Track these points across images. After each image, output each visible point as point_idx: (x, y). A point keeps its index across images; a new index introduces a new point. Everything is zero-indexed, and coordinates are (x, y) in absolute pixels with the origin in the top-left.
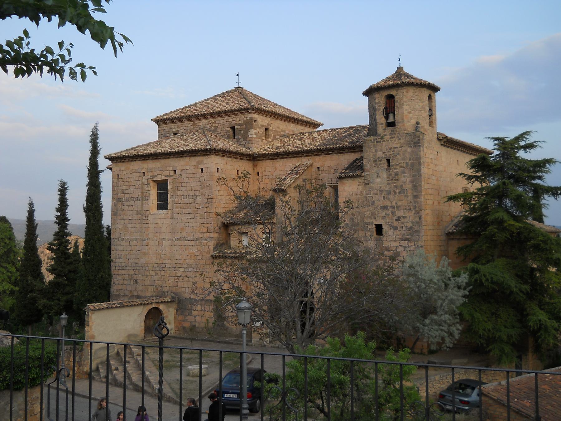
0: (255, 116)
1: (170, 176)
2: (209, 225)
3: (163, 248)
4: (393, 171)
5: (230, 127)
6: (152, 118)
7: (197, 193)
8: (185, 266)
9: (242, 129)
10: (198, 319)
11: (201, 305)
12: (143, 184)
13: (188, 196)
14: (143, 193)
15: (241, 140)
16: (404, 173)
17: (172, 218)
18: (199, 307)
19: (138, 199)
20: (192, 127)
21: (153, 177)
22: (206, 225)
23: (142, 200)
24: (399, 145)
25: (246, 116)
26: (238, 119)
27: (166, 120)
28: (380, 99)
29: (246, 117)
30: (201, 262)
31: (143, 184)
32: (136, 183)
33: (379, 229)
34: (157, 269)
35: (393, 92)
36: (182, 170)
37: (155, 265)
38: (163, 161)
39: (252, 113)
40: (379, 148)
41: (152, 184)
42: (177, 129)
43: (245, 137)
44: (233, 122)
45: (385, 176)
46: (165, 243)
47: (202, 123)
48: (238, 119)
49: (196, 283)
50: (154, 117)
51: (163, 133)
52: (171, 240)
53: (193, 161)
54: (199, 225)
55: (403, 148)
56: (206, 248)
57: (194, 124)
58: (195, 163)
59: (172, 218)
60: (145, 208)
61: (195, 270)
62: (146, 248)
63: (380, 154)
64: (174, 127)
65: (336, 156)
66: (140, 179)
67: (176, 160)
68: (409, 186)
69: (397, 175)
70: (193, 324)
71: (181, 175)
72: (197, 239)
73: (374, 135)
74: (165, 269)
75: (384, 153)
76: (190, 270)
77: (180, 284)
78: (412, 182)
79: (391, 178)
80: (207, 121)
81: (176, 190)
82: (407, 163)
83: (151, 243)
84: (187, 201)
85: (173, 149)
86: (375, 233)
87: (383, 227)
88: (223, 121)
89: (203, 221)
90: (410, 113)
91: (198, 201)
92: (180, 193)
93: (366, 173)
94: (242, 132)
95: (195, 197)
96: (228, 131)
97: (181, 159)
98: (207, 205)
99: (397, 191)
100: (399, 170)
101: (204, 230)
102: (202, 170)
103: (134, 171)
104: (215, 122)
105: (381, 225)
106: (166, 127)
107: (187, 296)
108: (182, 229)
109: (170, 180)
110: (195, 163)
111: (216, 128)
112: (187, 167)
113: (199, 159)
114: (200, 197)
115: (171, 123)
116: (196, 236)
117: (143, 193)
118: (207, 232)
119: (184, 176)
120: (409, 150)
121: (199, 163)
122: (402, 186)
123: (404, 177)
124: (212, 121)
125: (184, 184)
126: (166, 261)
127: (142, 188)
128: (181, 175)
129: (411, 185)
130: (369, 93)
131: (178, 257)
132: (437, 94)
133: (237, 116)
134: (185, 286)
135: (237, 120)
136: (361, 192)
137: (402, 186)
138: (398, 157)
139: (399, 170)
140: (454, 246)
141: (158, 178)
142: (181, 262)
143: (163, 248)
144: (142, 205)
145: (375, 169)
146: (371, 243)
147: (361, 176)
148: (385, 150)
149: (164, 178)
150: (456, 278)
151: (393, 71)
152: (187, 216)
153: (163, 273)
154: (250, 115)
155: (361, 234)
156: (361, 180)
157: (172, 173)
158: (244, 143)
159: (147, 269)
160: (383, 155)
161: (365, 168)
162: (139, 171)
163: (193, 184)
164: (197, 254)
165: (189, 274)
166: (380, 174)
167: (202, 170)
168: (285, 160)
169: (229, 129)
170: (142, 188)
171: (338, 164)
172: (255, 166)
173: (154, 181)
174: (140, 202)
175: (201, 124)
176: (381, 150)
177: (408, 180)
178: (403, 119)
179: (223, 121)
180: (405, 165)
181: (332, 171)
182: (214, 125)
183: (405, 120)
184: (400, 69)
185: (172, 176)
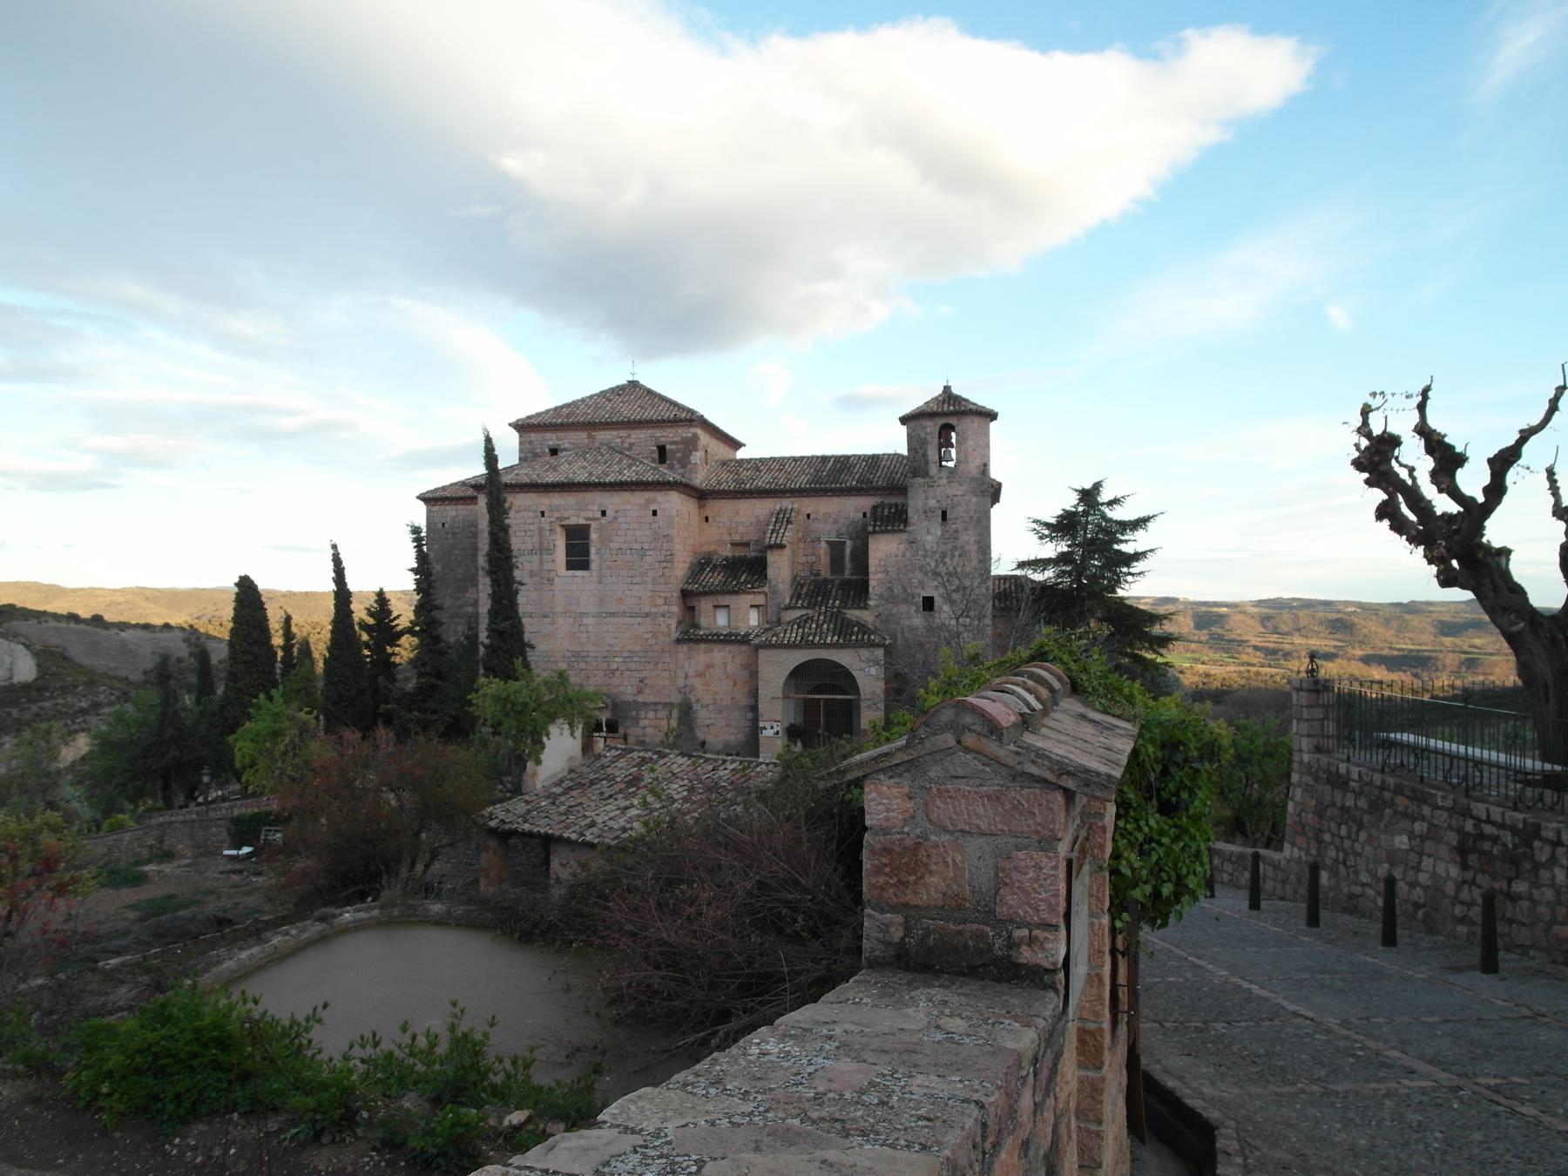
0: (699, 431)
1: (595, 519)
2: (669, 595)
3: (583, 628)
4: (951, 527)
5: (658, 447)
6: (511, 421)
7: (646, 546)
8: (626, 654)
9: (679, 450)
10: (649, 731)
11: (656, 711)
12: (541, 529)
13: (628, 551)
14: (541, 543)
15: (677, 466)
16: (966, 529)
17: (600, 582)
18: (651, 714)
19: (531, 552)
20: (586, 441)
21: (562, 519)
22: (663, 595)
23: (541, 554)
24: (959, 493)
25: (686, 430)
26: (671, 435)
27: (539, 425)
28: (932, 427)
29: (687, 432)
30: (655, 648)
31: (541, 529)
32: (527, 527)
33: (928, 604)
34: (573, 659)
35: (953, 421)
36: (617, 511)
37: (568, 654)
38: (581, 495)
39: (696, 426)
40: (931, 494)
41: (559, 530)
42: (556, 442)
43: (684, 462)
44: (663, 439)
45: (939, 533)
46: (585, 621)
47: (603, 436)
48: (671, 435)
49: (645, 678)
50: (513, 420)
51: (528, 446)
52: (599, 615)
53: (639, 498)
54: (650, 594)
55: (966, 497)
56: (664, 628)
57: (589, 436)
58: (642, 502)
59: (600, 582)
60: (547, 566)
61: (644, 660)
62: (551, 628)
63: (932, 503)
64: (552, 439)
65: (836, 500)
66: (536, 521)
67: (606, 494)
68: (973, 548)
69: (956, 531)
70: (641, 738)
71: (615, 518)
72: (647, 615)
73: (924, 477)
74: (589, 660)
75: (938, 502)
76: (634, 659)
77: (615, 681)
78: (978, 542)
79: (947, 536)
80: (614, 433)
81: (605, 541)
82: (971, 517)
83: (560, 621)
84: (628, 558)
85: (719, 483)
86: (921, 608)
87: (936, 599)
88: (643, 436)
89: (658, 587)
90: (974, 450)
91: (649, 559)
92: (612, 545)
93: (911, 528)
94: (679, 455)
95: (642, 553)
96: (652, 452)
97: (615, 494)
98: (665, 564)
99: (957, 553)
100: (959, 525)
101: (660, 601)
102: (655, 513)
103: (522, 508)
104: (629, 436)
105: (932, 598)
106: (533, 436)
107: (630, 699)
108: (619, 600)
109: (594, 525)
110: (642, 502)
111: (631, 445)
112: (627, 507)
113: (648, 495)
114: (652, 553)
115: (548, 431)
116: (646, 609)
117: (541, 543)
118: (665, 604)
119: (620, 520)
120: (974, 500)
121: (648, 502)
122: (963, 547)
123: (967, 535)
124: (623, 433)
125: (622, 533)
126: (590, 648)
127: (541, 535)
128: (615, 518)
129: (976, 546)
130: (904, 420)
131: (612, 641)
132: (993, 425)
133: (669, 430)
134: (625, 683)
135: (669, 436)
136: (904, 553)
137: (963, 547)
138: (959, 508)
139: (959, 525)
140: (182, 650)
141: (573, 521)
142: (617, 648)
143: (583, 628)
144: (541, 562)
145: (925, 523)
146: (918, 621)
147: (904, 531)
148: (940, 498)
149: (582, 521)
150: (52, 722)
151: (938, 391)
152: (629, 580)
153: (583, 665)
154: (693, 430)
155: (903, 608)
156: (904, 536)
157: (599, 514)
158: (682, 471)
159: (552, 659)
160: (938, 505)
161: (910, 520)
162: (534, 508)
163: (637, 533)
164: (646, 636)
165: (632, 666)
166: (932, 530)
167: (655, 513)
168: (753, 501)
169: (655, 448)
170: (541, 535)
171: (839, 512)
172: (701, 507)
173: (563, 526)
174: (536, 558)
175: (603, 437)
176: (934, 498)
177: (972, 539)
178: (966, 458)
179: (643, 436)
180: (968, 520)
181: (831, 520)
182: (628, 441)
183: (970, 460)
184: (947, 389)
185: (597, 519)
